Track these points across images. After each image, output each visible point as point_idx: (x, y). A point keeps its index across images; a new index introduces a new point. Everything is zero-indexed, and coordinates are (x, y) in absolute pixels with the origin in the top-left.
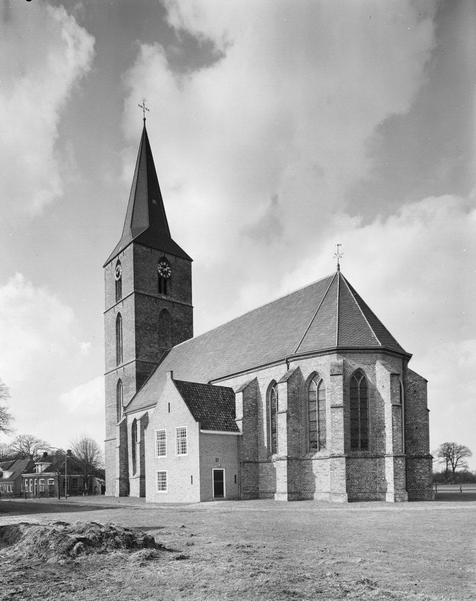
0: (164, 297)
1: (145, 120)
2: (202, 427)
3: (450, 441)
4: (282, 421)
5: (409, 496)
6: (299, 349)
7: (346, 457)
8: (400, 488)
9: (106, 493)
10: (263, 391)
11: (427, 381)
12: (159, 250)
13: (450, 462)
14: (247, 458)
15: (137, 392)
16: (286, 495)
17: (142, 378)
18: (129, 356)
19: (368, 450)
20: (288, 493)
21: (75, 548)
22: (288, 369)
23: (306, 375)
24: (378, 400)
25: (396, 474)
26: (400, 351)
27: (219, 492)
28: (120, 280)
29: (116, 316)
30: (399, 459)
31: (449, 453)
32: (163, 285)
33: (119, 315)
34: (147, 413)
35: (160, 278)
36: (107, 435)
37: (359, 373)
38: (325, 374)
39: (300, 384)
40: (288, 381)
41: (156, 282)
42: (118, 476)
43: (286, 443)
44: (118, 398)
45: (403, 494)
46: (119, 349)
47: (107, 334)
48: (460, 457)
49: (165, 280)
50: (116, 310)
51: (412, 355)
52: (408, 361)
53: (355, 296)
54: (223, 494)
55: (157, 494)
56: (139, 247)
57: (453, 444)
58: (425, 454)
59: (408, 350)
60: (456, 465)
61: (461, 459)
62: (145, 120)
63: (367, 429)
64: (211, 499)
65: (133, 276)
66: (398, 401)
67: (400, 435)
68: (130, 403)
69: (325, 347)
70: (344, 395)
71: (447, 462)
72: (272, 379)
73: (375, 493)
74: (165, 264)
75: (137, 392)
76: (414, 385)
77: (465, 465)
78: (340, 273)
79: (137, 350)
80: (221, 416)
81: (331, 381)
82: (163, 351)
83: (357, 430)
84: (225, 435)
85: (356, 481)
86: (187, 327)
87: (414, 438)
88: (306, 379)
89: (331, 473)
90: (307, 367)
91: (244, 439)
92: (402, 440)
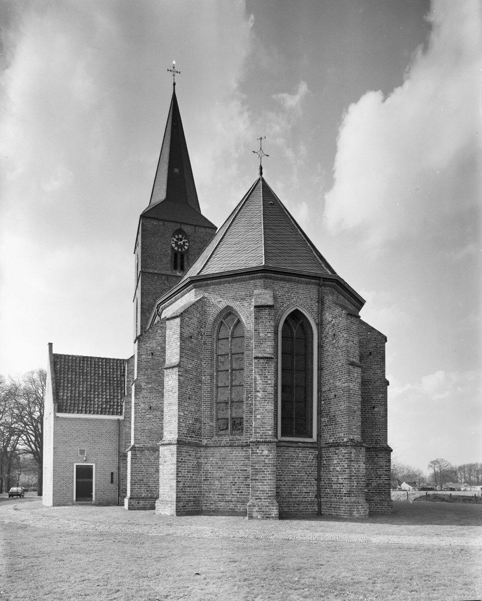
1: (174, 84)
5: (280, 506)
8: (263, 496)
12: (173, 222)
27: (84, 493)
32: (179, 261)
35: (175, 254)
45: (267, 506)
62: (174, 84)
64: (70, 503)
84: (91, 420)
85: (217, 482)
87: (332, 414)
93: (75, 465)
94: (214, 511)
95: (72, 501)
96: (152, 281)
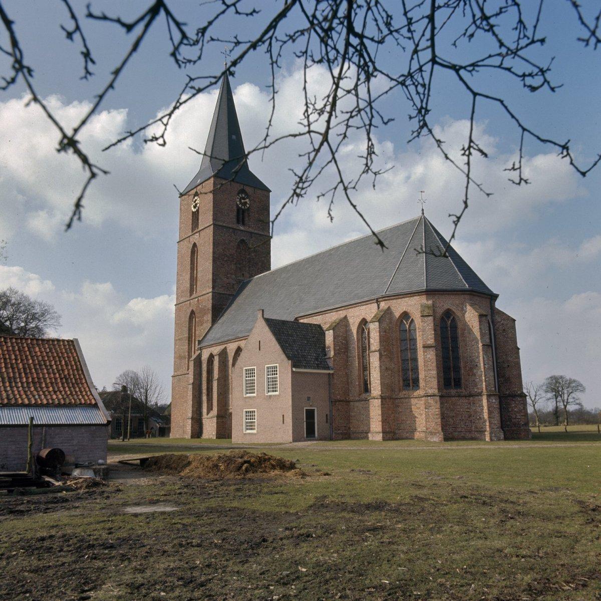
0: (242, 228)
2: (294, 366)
3: (557, 373)
4: (375, 361)
6: (389, 289)
7: (440, 396)
9: (171, 435)
10: (354, 329)
11: (515, 320)
13: (559, 398)
14: (338, 397)
15: (213, 325)
16: (381, 435)
17: (219, 309)
18: (205, 289)
19: (461, 389)
20: (383, 433)
21: (244, 468)
22: (379, 308)
23: (397, 314)
24: (468, 339)
25: (490, 412)
26: (487, 292)
27: (310, 433)
28: (198, 211)
29: (191, 246)
30: (493, 397)
31: (558, 388)
33: (195, 245)
34: (226, 348)
35: (239, 209)
36: (175, 371)
37: (448, 313)
38: (416, 315)
39: (391, 323)
40: (379, 321)
41: (235, 213)
42: (190, 415)
43: (379, 381)
44: (190, 329)
46: (193, 280)
47: (180, 263)
48: (571, 393)
49: (244, 211)
50: (191, 240)
51: (498, 295)
52: (495, 300)
53: (440, 239)
54: (314, 434)
55: (245, 434)
56: (219, 181)
57: (561, 377)
58: (519, 392)
59: (495, 291)
60: (567, 403)
61: (573, 395)
63: (460, 368)
64: (303, 439)
65: (212, 208)
66: (488, 340)
67: (492, 374)
68: (205, 337)
69: (414, 289)
70: (435, 334)
71: (556, 398)
72: (362, 318)
73: (470, 432)
74: (244, 196)
75: (213, 325)
76: (503, 324)
77: (578, 402)
78: (424, 217)
79: (214, 281)
80: (311, 353)
81: (422, 322)
82: (240, 282)
83: (449, 369)
84: (307, 373)
85: (450, 420)
86: (264, 257)
88: (397, 317)
89: (426, 412)
90: (399, 307)
91: (335, 376)
92: (495, 379)
93: (255, 410)
94: (451, 438)
95: (304, 438)
96: (222, 233)
